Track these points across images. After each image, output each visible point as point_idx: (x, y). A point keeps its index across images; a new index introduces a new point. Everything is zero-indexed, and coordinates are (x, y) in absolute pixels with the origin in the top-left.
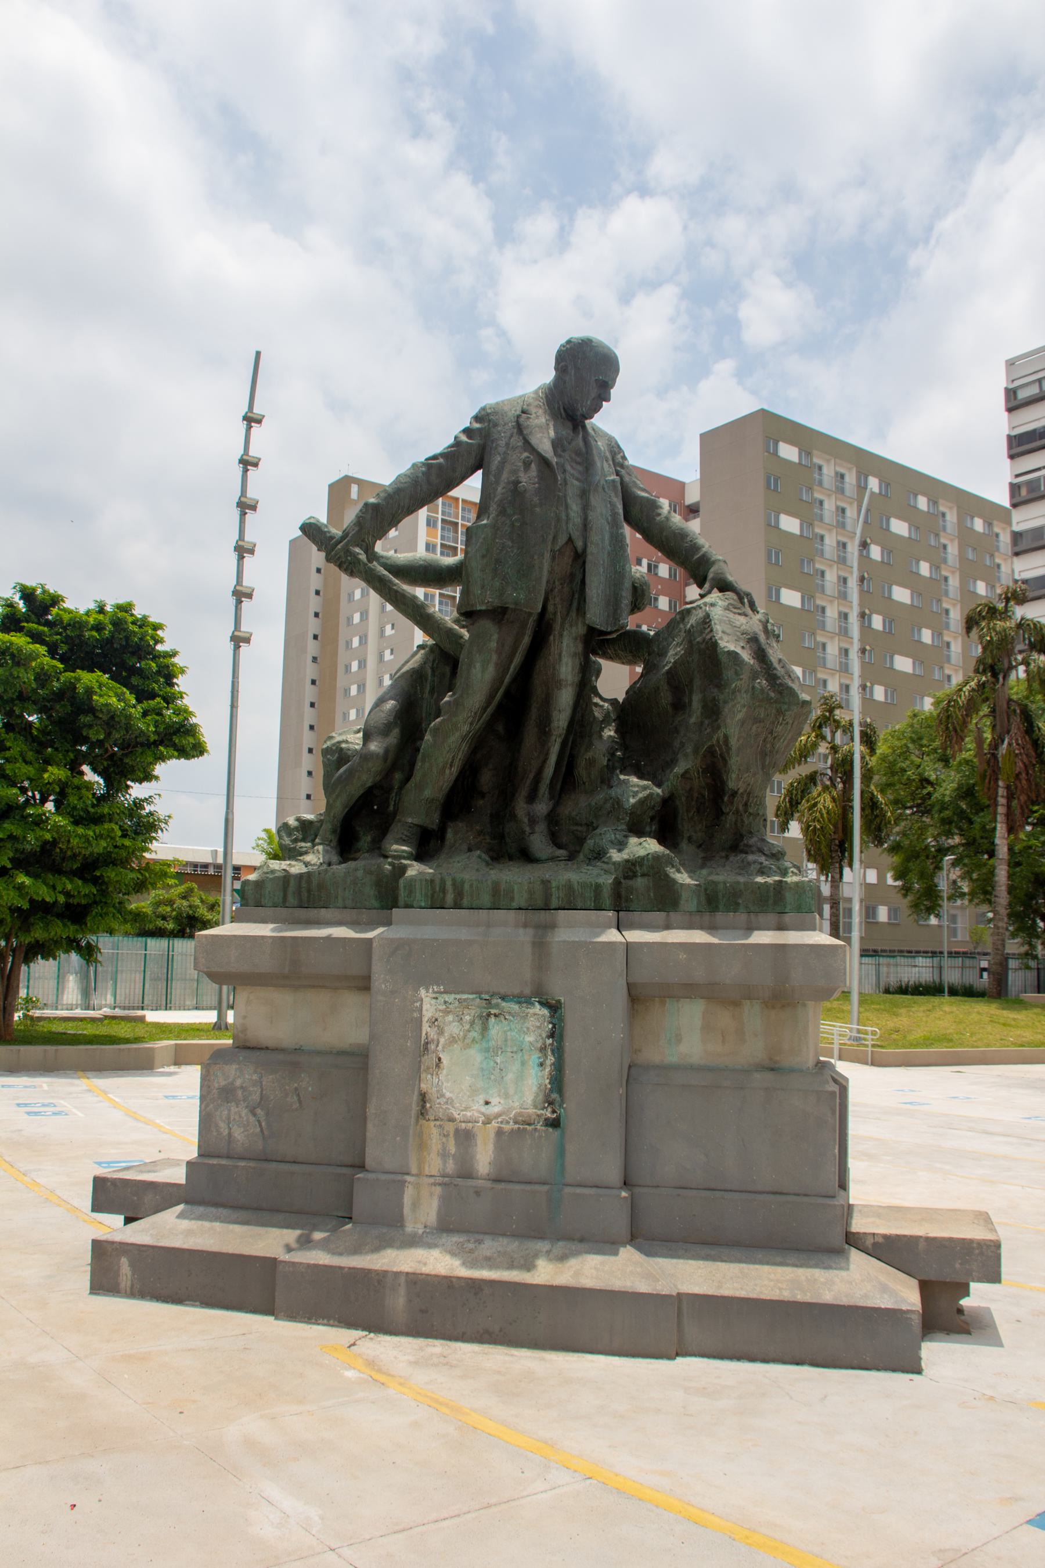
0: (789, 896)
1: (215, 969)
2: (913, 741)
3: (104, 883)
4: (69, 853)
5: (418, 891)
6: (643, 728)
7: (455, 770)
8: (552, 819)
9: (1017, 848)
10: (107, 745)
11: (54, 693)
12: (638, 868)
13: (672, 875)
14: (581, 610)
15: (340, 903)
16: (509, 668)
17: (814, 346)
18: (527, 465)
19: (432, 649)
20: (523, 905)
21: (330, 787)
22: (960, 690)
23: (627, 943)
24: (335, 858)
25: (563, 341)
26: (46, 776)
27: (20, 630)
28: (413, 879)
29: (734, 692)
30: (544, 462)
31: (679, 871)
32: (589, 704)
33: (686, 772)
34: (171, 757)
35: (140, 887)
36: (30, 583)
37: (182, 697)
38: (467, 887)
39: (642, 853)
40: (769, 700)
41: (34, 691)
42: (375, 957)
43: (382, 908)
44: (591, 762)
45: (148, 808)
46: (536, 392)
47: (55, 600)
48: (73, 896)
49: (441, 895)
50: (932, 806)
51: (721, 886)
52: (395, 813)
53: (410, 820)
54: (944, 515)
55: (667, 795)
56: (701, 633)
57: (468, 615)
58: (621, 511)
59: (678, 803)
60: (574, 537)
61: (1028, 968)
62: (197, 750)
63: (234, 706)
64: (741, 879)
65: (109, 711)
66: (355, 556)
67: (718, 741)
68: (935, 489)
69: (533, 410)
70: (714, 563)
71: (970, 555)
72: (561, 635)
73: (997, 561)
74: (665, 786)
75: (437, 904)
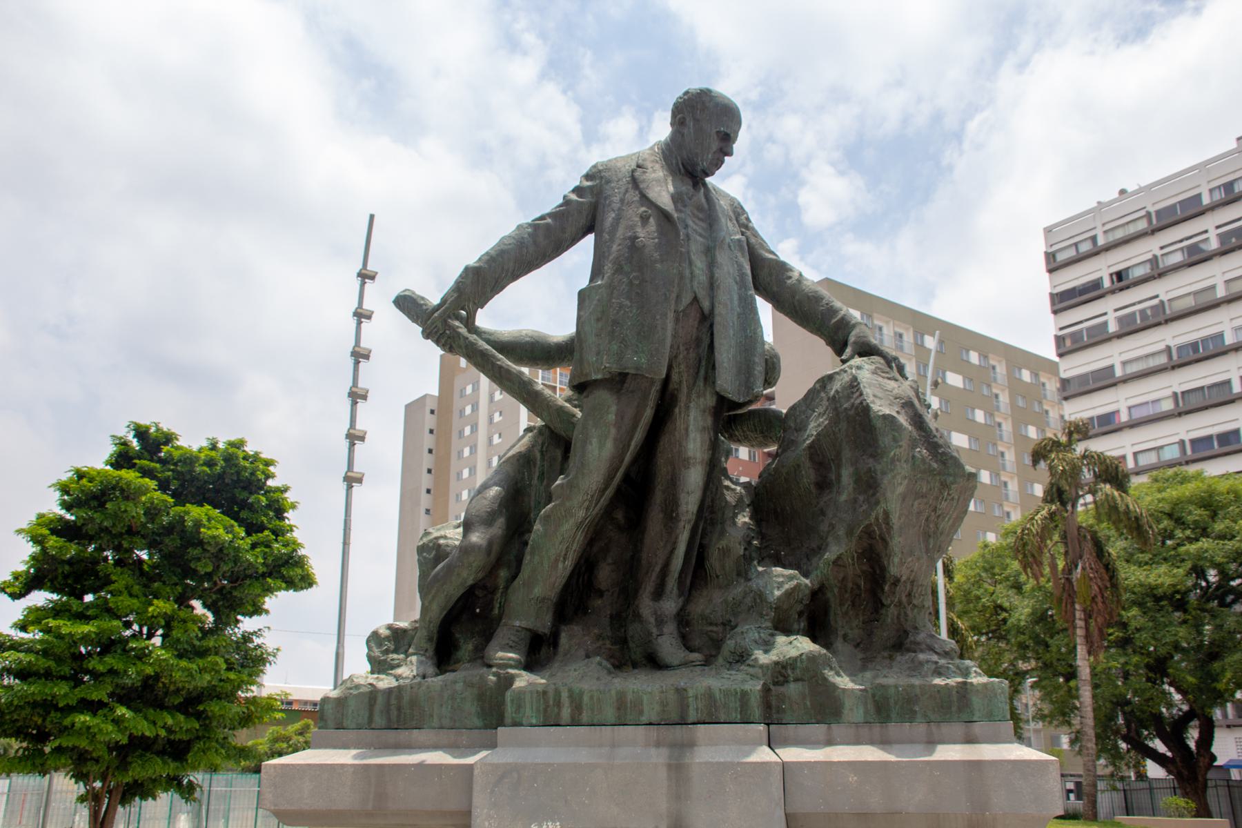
0: (976, 701)
1: (285, 806)
2: (986, 570)
3: (207, 717)
4: (172, 688)
5: (528, 705)
6: (782, 515)
7: (569, 564)
8: (683, 620)
9: (1099, 669)
10: (215, 578)
11: (163, 527)
12: (789, 672)
13: (831, 679)
14: (710, 379)
15: (436, 722)
16: (629, 446)
17: (866, 226)
18: (644, 219)
19: (541, 431)
20: (654, 719)
21: (426, 587)
22: (1033, 519)
23: (784, 764)
24: (431, 670)
25: (680, 93)
26: (151, 609)
27: (132, 466)
28: (521, 692)
29: (893, 461)
30: (664, 215)
31: (839, 675)
32: (720, 486)
33: (839, 558)
34: (279, 589)
35: (246, 720)
36: (144, 421)
37: (292, 530)
38: (586, 699)
39: (794, 653)
40: (931, 471)
41: (144, 525)
42: (477, 788)
43: (486, 727)
44: (725, 552)
45: (257, 641)
46: (652, 148)
47: (169, 438)
48: (175, 732)
49: (556, 710)
50: (1008, 631)
51: (892, 691)
52: (500, 617)
53: (517, 623)
54: (994, 368)
55: (816, 587)
56: (849, 397)
57: (581, 387)
58: (749, 272)
59: (829, 595)
60: (699, 296)
61: (1115, 789)
62: (306, 581)
63: (346, 543)
64: (916, 682)
65: (217, 544)
66: (454, 329)
67: (877, 519)
68: (986, 345)
69: (649, 165)
70: (854, 326)
71: (1021, 403)
72: (688, 408)
73: (1045, 407)
74: (813, 576)
75: (550, 720)
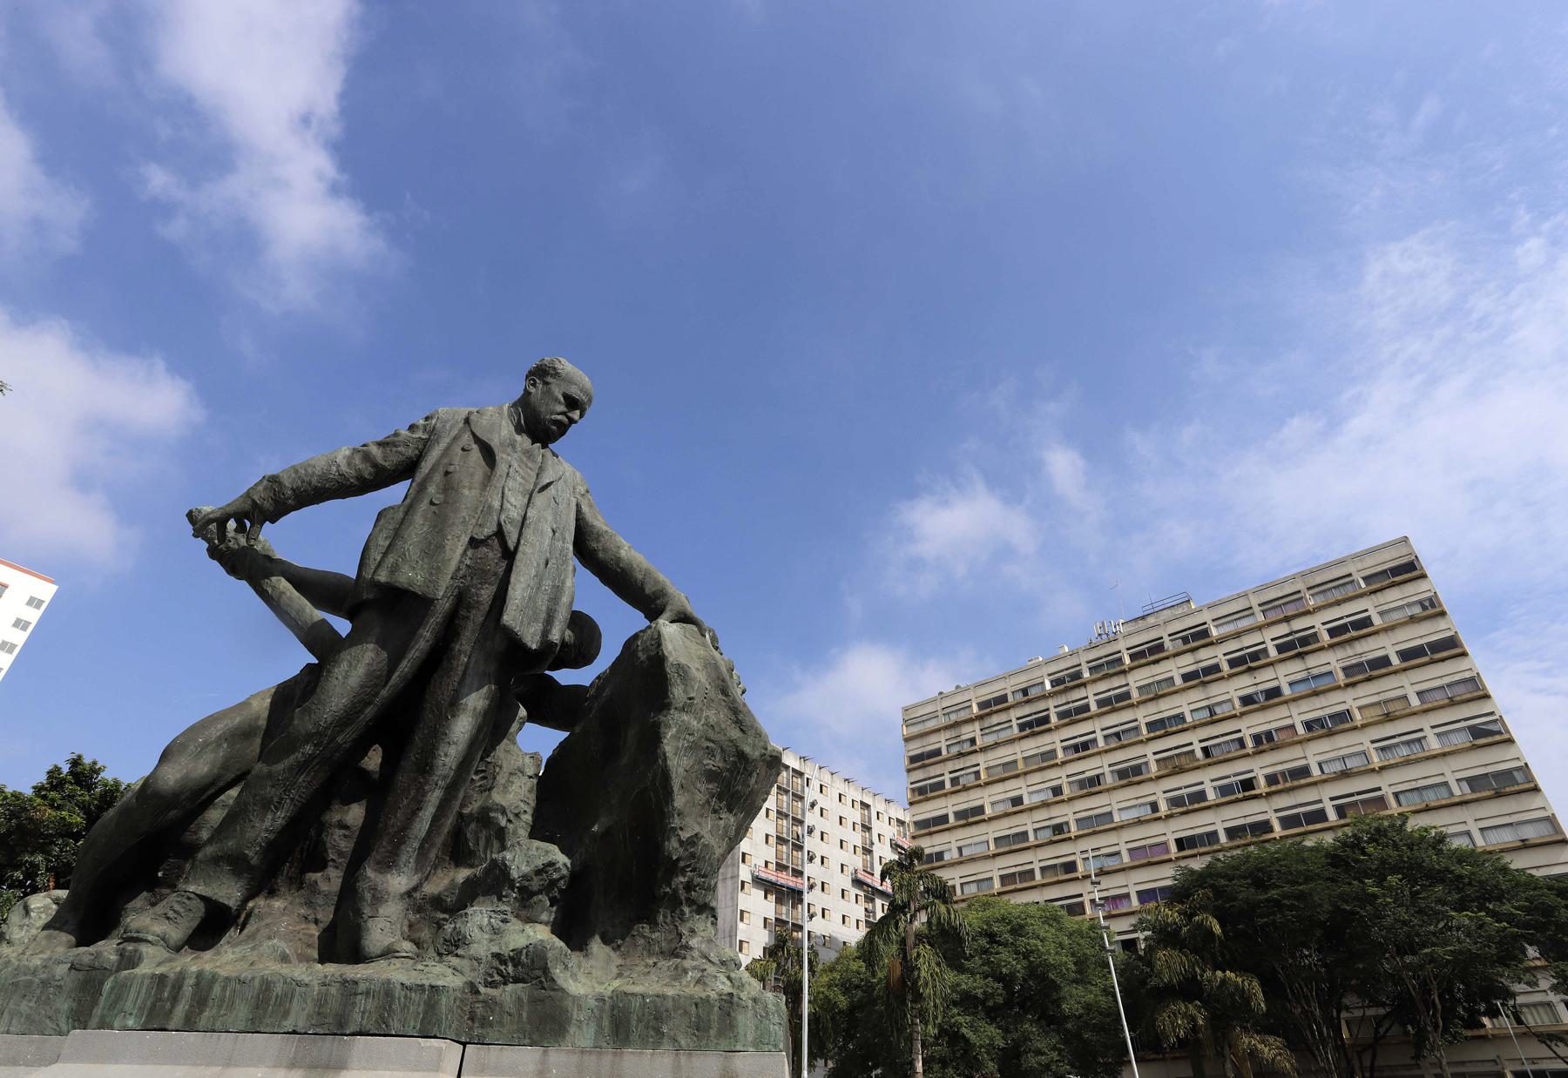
5: (132, 995)
